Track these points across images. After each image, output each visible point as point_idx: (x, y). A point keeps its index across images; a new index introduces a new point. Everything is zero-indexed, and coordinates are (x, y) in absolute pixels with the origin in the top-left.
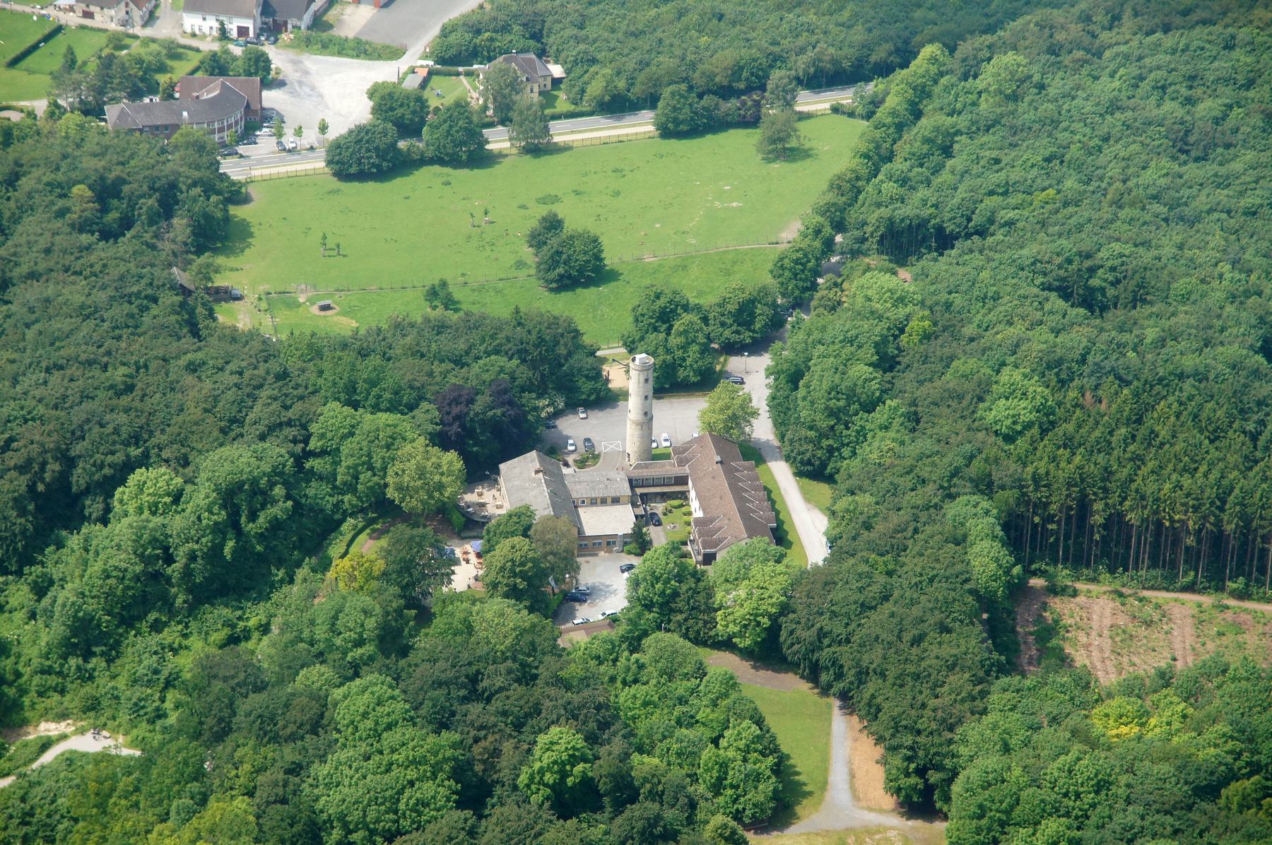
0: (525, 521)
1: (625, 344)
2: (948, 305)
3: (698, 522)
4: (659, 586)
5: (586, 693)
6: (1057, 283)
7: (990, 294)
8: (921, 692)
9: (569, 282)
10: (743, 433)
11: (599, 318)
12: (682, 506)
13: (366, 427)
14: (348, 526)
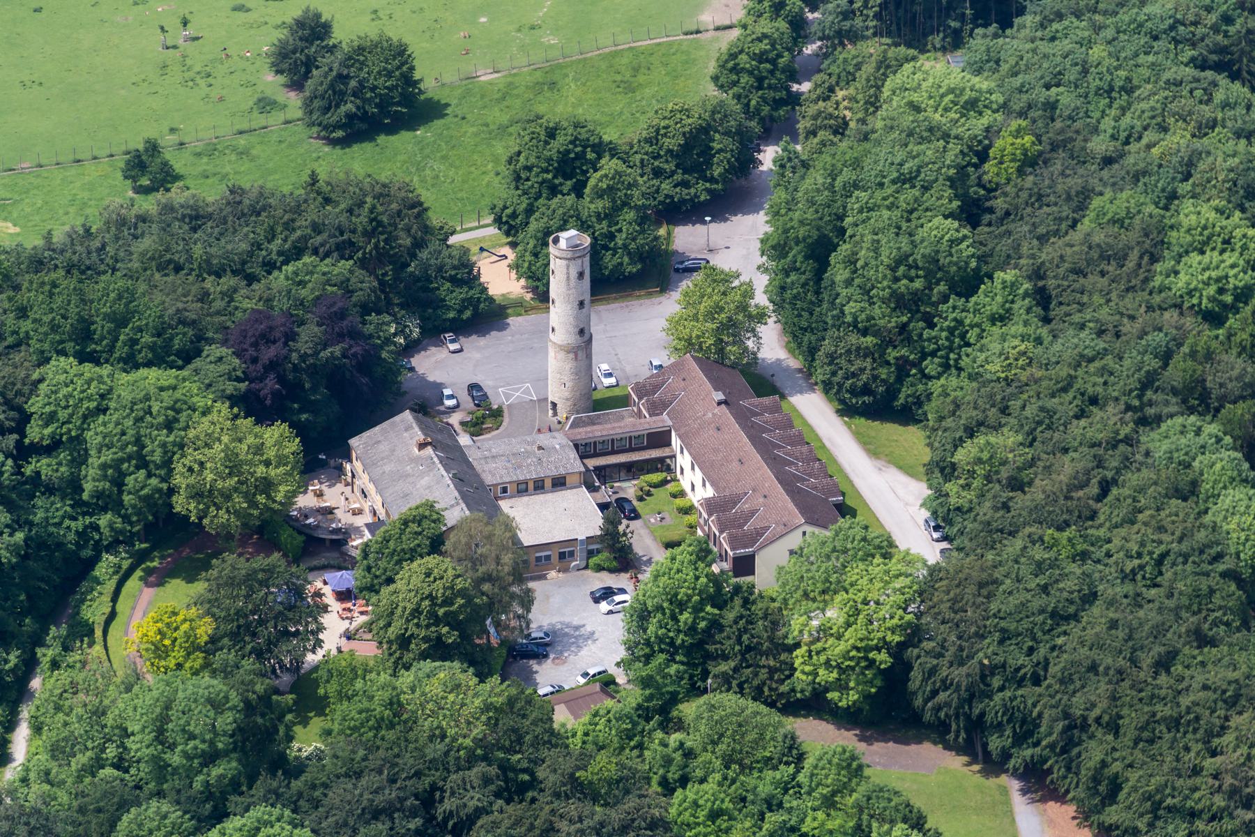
0: (429, 529)
1: (498, 221)
2: (1051, 106)
4: (685, 617)
5: (631, 803)
6: (1214, 57)
7: (1118, 84)
8: (1187, 749)
9: (364, 126)
10: (746, 349)
11: (454, 183)
12: (664, 482)
13: (126, 395)
14: (106, 566)
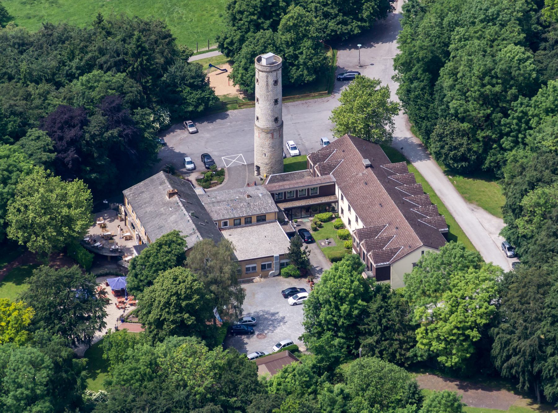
1: (221, 47)
3: (361, 234)
4: (345, 307)
10: (384, 131)
12: (331, 219)
